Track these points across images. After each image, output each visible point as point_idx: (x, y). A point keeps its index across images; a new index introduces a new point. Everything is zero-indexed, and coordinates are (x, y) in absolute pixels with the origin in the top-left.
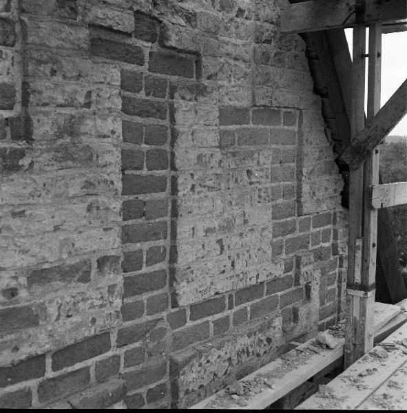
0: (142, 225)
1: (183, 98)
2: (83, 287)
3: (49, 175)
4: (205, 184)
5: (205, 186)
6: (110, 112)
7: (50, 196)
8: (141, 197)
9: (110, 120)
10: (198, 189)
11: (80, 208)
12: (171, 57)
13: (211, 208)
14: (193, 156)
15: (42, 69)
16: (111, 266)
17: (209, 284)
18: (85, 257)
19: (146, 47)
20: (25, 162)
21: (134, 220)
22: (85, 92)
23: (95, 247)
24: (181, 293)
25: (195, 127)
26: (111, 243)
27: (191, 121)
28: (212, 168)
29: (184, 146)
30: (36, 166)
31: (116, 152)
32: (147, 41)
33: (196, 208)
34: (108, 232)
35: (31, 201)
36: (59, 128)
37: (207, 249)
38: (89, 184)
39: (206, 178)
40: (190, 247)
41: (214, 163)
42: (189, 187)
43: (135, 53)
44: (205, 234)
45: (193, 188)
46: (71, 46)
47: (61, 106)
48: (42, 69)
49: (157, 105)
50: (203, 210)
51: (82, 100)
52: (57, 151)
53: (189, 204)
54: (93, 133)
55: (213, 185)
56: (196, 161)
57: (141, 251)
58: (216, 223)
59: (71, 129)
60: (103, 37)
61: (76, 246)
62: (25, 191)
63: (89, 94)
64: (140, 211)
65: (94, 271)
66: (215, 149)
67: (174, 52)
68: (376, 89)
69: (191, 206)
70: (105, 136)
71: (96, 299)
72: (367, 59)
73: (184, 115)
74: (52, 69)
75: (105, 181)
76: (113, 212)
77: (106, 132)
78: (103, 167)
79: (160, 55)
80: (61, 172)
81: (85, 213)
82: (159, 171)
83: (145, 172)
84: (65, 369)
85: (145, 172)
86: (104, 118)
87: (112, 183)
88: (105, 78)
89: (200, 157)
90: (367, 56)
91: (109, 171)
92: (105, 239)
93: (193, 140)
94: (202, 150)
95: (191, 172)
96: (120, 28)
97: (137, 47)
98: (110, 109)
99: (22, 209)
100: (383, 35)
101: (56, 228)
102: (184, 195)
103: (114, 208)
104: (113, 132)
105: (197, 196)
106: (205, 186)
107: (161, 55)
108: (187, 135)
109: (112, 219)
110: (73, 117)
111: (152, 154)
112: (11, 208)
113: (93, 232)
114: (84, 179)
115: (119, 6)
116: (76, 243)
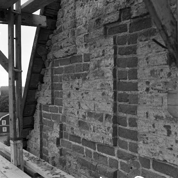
0: (126, 105)
1: (141, 41)
2: (100, 123)
3: (93, 81)
4: (155, 88)
5: (155, 89)
6: (110, 56)
7: (93, 88)
8: (127, 92)
9: (110, 59)
10: (151, 90)
11: (100, 93)
12: (140, 21)
13: (160, 104)
14: (147, 71)
15: (92, 47)
16: (109, 118)
17: (158, 151)
18: (101, 112)
19: (127, 22)
20: (87, 77)
21: (124, 103)
22: (102, 51)
23: (104, 110)
24: (139, 147)
25: (149, 55)
26: (109, 109)
27: (147, 52)
28: (161, 78)
29: (142, 66)
30: (90, 78)
31: (111, 72)
32: (128, 19)
33: (148, 101)
34: (109, 105)
35: (88, 89)
36: (95, 65)
37: (156, 128)
38: (102, 85)
39: (156, 84)
40: (144, 123)
41: (163, 74)
42: (145, 89)
43: (123, 28)
44: (155, 118)
45: (147, 90)
46: (98, 36)
47: (96, 57)
48: (92, 47)
49: (133, 48)
50: (154, 104)
51: (101, 54)
52: (94, 73)
53: (144, 98)
54: (104, 65)
55: (161, 89)
56: (149, 74)
57: (126, 118)
58: (163, 113)
59: (97, 66)
60: (112, 27)
61: (99, 107)
62: (87, 86)
63: (104, 51)
64: (126, 99)
65: (104, 119)
66: (164, 66)
67: (140, 18)
68: (11, 47)
69: (145, 100)
70: (108, 66)
71: (104, 130)
72: (15, 37)
73: (142, 49)
74: (94, 46)
75: (107, 84)
76: (110, 97)
77: (108, 64)
78: (107, 78)
79: (134, 23)
80: (95, 80)
81: (101, 96)
82: (134, 80)
83: (127, 81)
84: (100, 153)
85: (127, 81)
86: (108, 59)
87: (109, 85)
88: (108, 43)
89: (152, 72)
90: (15, 38)
91: (108, 80)
92: (107, 107)
93: (148, 62)
94: (154, 67)
95: (147, 80)
96: (113, 21)
97: (124, 24)
98: (109, 55)
99: (88, 92)
100: (22, 26)
101: (94, 99)
102: (141, 93)
103: (110, 95)
104: (110, 64)
105: (149, 95)
106: (155, 89)
107: (135, 22)
108: (143, 60)
109: (109, 99)
110: (99, 60)
111: (130, 72)
112: (84, 91)
113: (104, 103)
114: (101, 83)
115: (113, 12)
116: (99, 106)
